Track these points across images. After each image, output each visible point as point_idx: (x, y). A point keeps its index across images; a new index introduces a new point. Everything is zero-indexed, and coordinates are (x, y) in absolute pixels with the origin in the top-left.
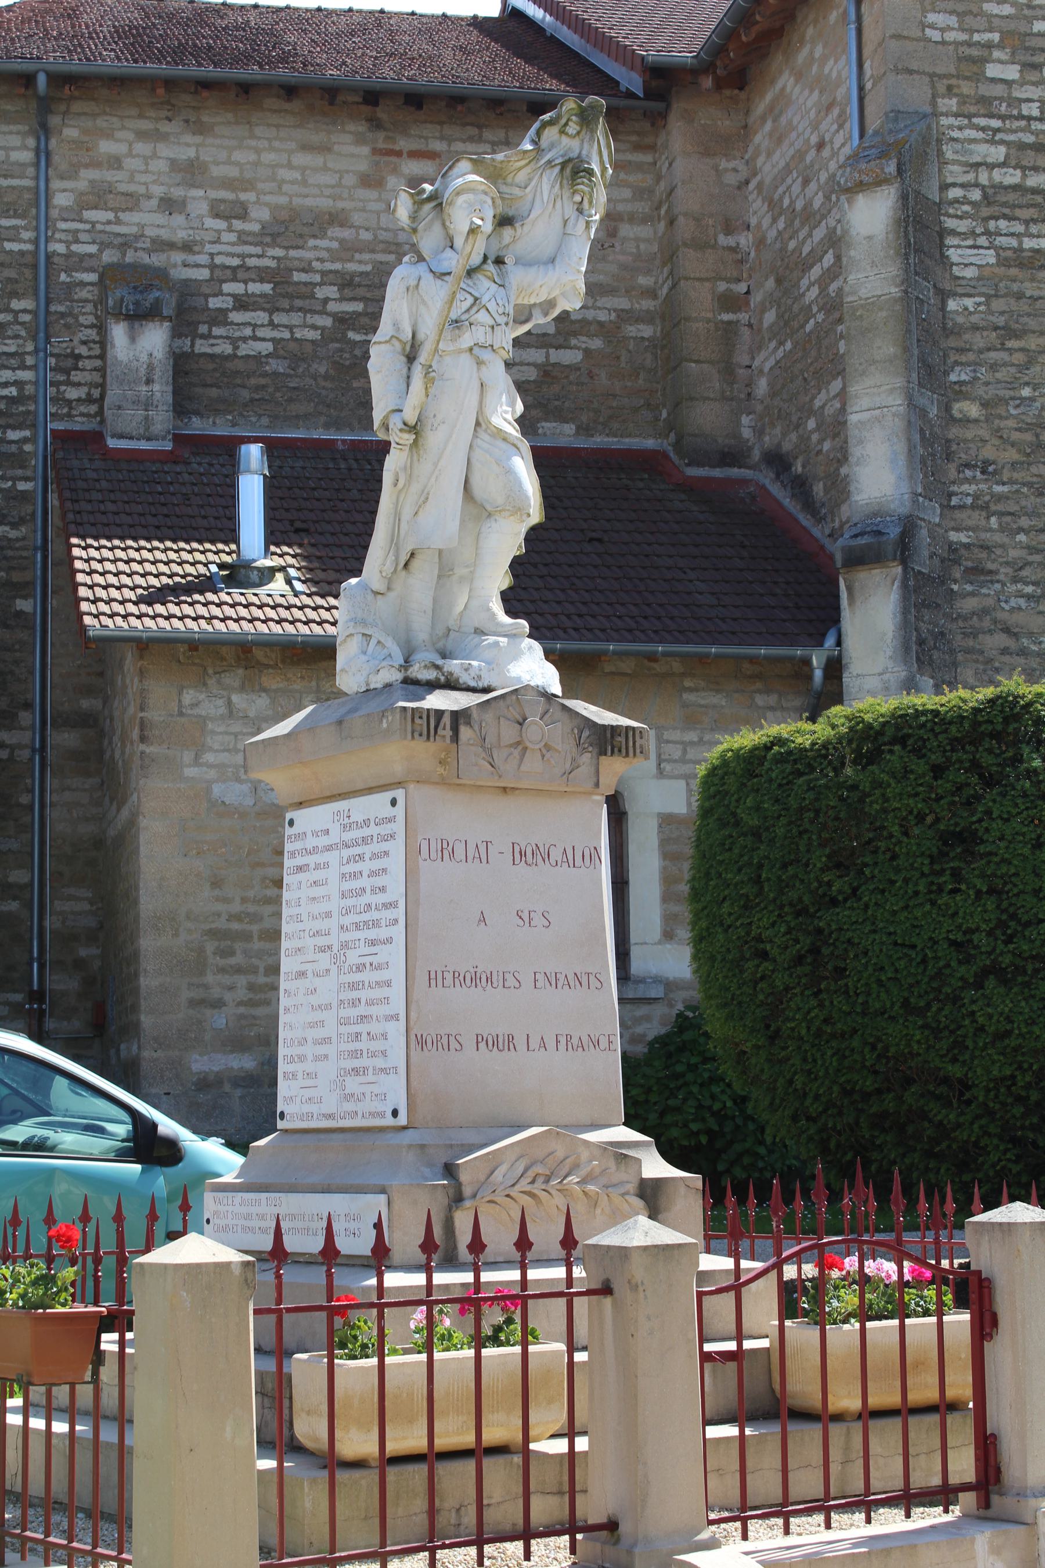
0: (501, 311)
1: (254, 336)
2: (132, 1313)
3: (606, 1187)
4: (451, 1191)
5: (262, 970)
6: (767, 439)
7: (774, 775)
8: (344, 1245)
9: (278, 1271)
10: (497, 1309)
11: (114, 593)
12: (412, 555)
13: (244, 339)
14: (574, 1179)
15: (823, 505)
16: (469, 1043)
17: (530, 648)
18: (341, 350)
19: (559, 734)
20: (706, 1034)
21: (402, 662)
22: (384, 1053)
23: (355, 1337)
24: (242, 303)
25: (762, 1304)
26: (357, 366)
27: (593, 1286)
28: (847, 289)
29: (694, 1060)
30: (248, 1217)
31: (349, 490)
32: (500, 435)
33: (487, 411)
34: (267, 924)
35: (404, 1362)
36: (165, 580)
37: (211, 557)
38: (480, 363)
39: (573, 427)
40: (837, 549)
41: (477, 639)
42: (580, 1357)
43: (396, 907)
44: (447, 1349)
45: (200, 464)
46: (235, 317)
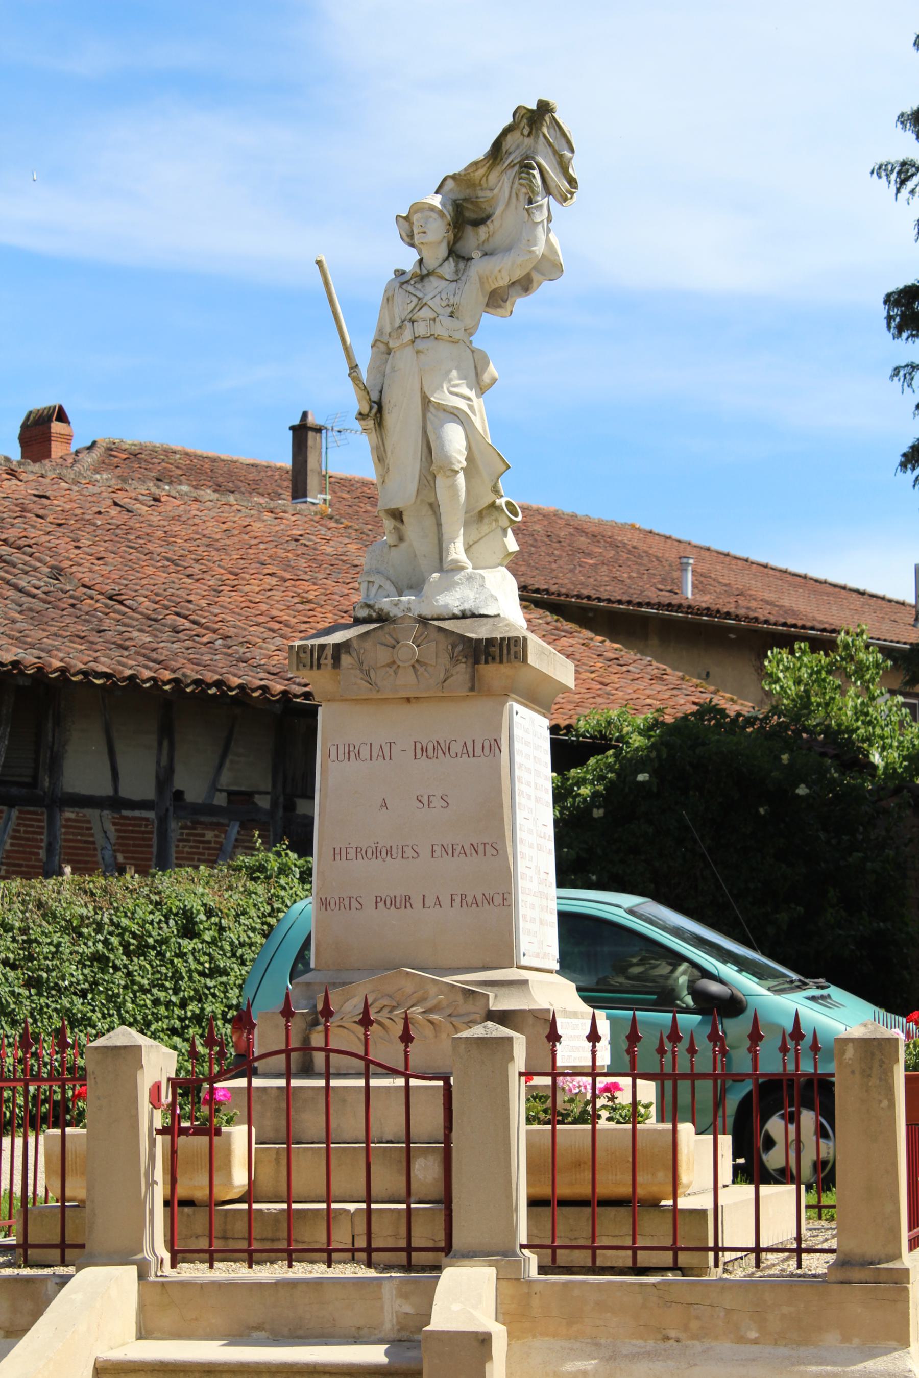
16: (369, 902)
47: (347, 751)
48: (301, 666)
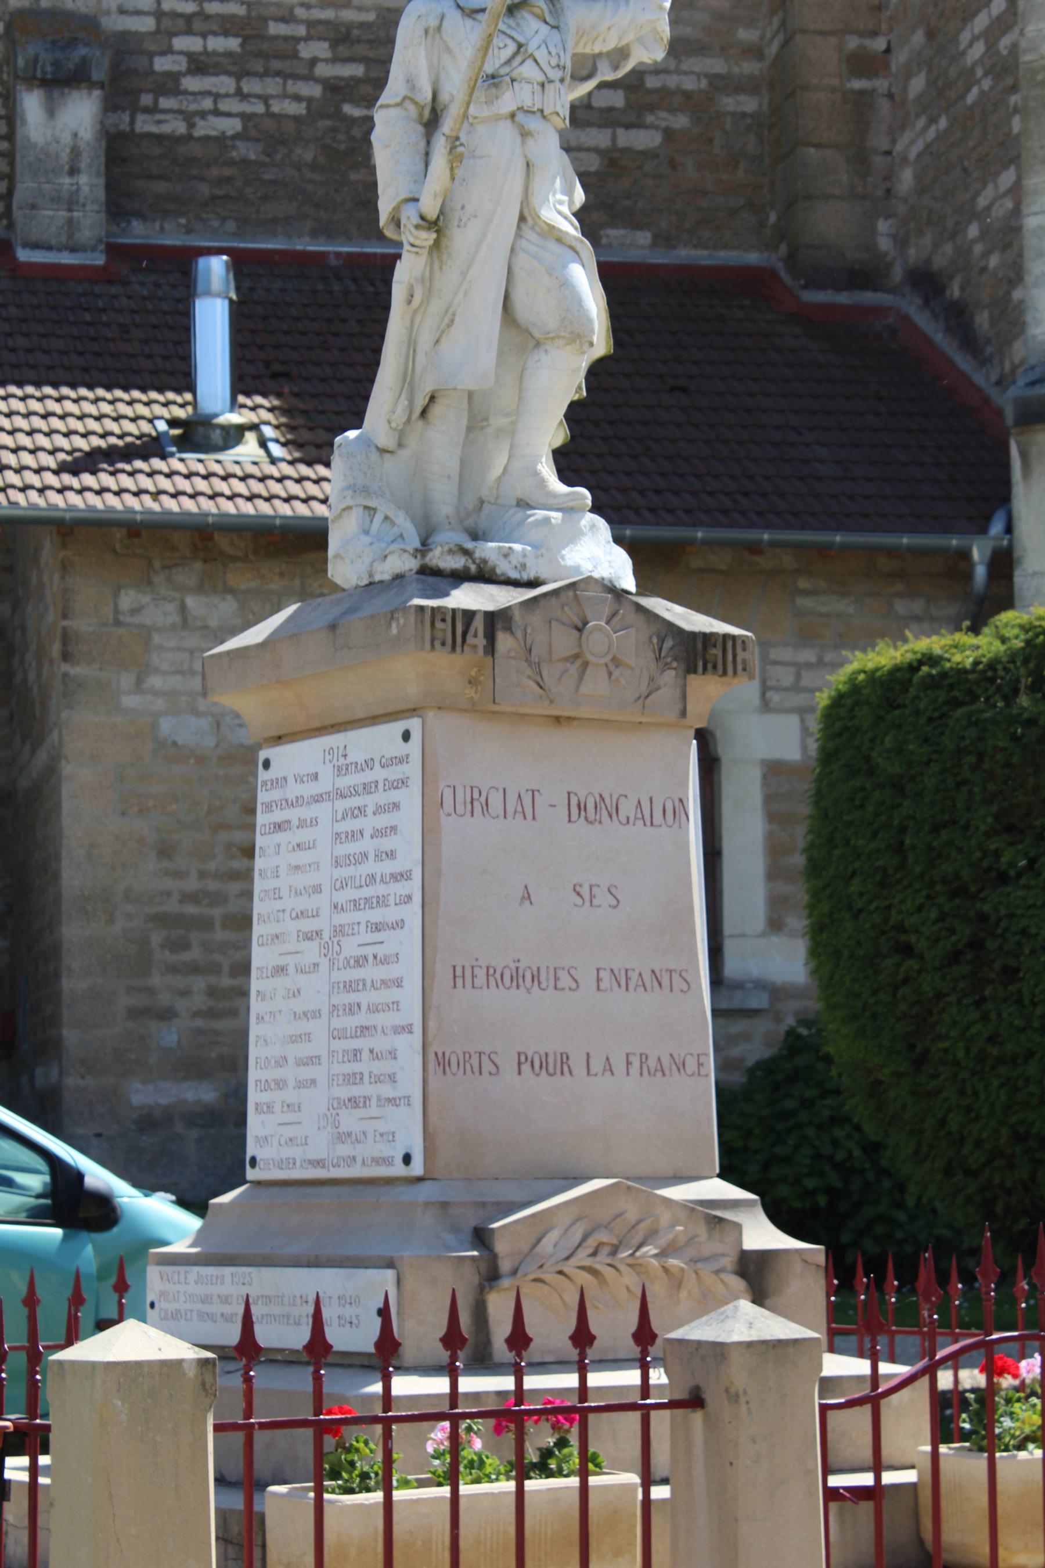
0: (554, 62)
1: (216, 110)
2: (47, 1428)
3: (694, 1261)
4: (483, 1266)
5: (226, 969)
6: (912, 251)
7: (922, 705)
8: (338, 1338)
9: (247, 1373)
10: (545, 1426)
11: (27, 459)
12: (432, 398)
13: (203, 114)
14: (650, 1250)
15: (988, 341)
16: (508, 1066)
17: (593, 526)
18: (334, 130)
19: (631, 643)
20: (828, 1059)
21: (417, 544)
22: (392, 1078)
23: (352, 1464)
24: (199, 65)
25: (909, 1424)
26: (356, 152)
27: (678, 1396)
28: (1023, 44)
29: (809, 1093)
30: (206, 1299)
31: (344, 321)
32: (552, 233)
33: (535, 201)
34: (234, 907)
35: (419, 1498)
36: (96, 441)
37: (158, 410)
38: (525, 134)
39: (648, 235)
40: (1007, 401)
41: (520, 514)
42: (660, 1492)
43: (409, 878)
44: (477, 1481)
45: (142, 284)
46: (191, 83)
47: (469, 799)
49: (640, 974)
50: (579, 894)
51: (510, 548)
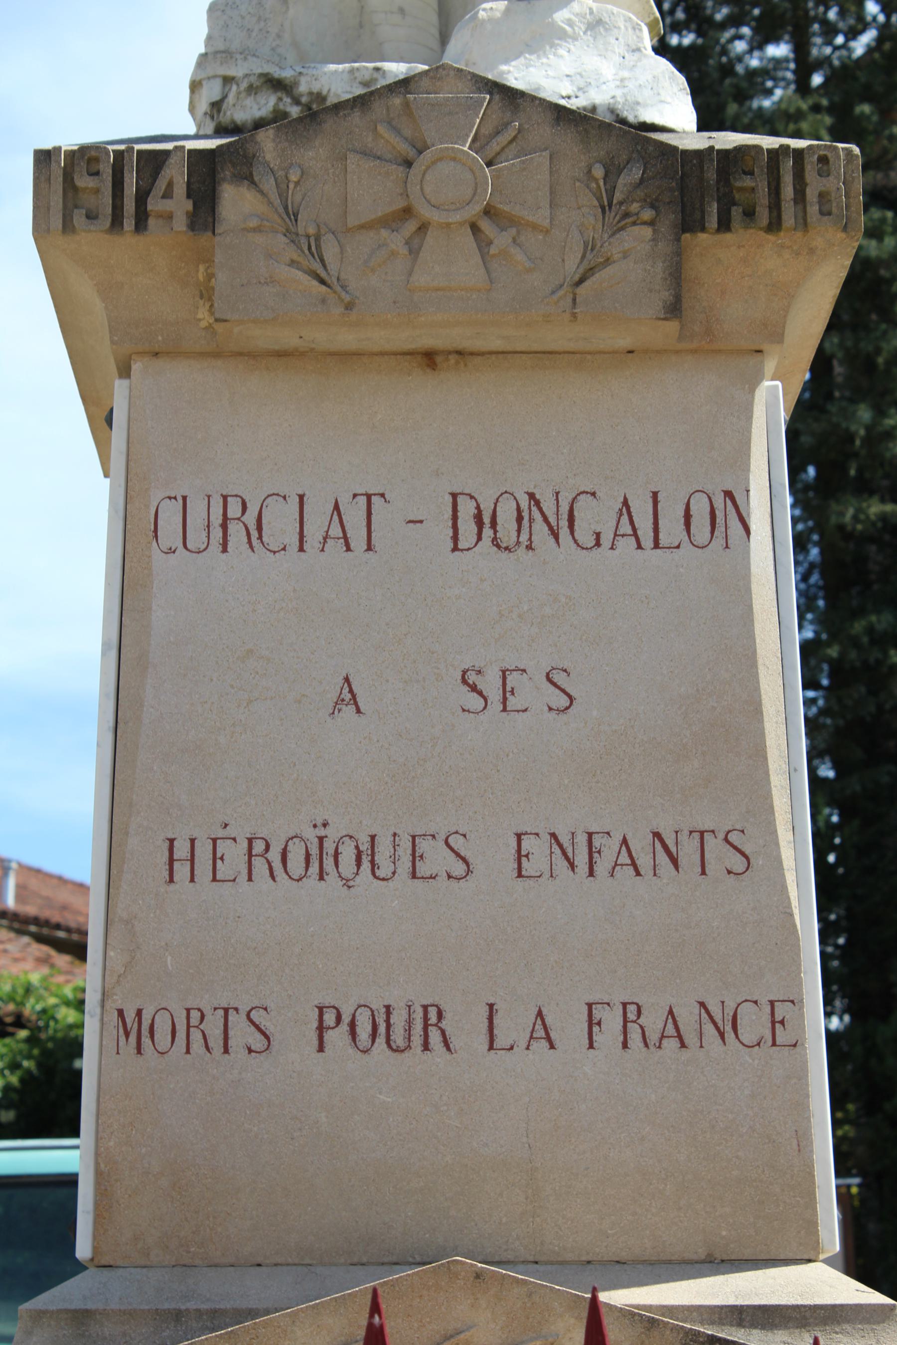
16: (293, 1030)
48: (79, 218)
49: (625, 841)
50: (474, 688)
51: (377, 69)
